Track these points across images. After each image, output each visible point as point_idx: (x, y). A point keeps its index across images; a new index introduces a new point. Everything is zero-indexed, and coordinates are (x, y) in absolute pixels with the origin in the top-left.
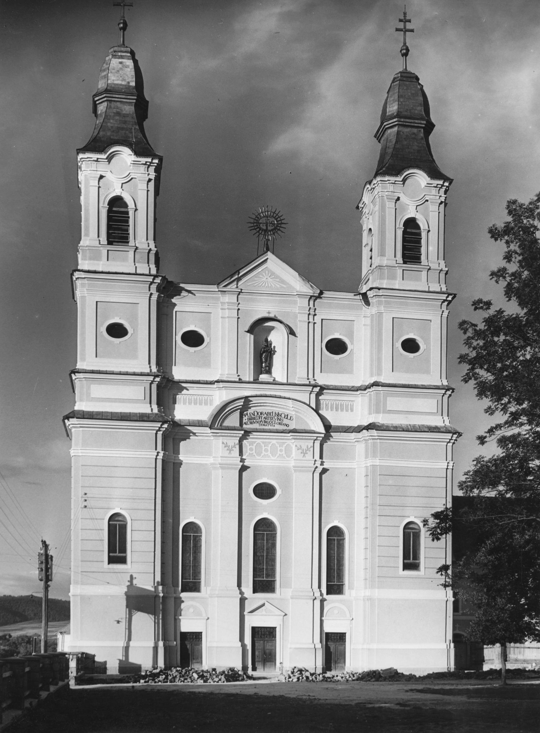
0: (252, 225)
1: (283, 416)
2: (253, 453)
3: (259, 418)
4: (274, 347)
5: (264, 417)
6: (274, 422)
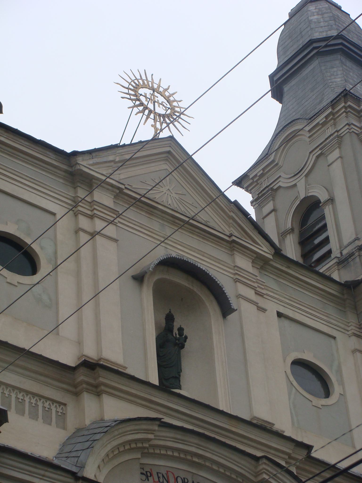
0: (126, 91)
4: (181, 330)
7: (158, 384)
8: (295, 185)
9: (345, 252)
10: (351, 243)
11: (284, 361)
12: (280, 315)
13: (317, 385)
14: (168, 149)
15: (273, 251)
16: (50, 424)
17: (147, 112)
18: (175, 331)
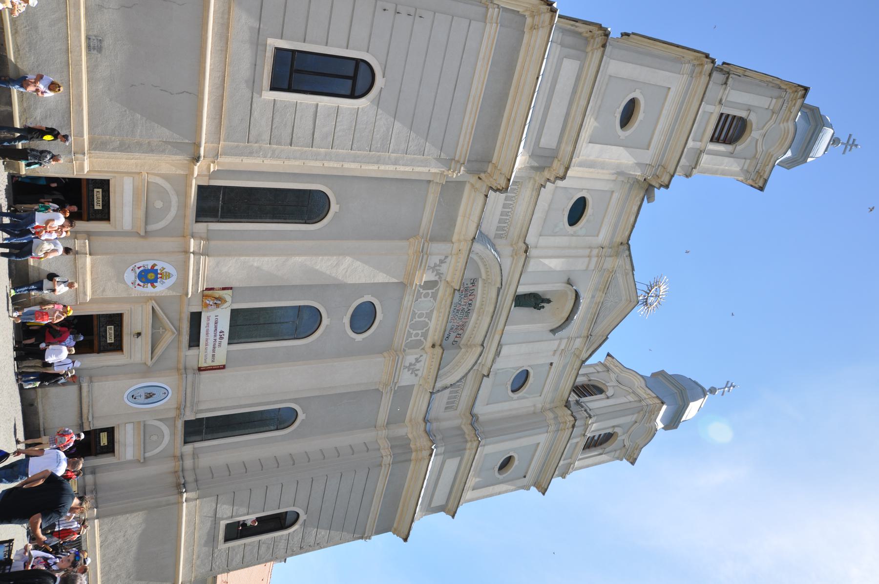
1: (460, 332)
2: (415, 318)
3: (465, 302)
4: (543, 307)
5: (464, 309)
6: (455, 321)
7: (458, 458)
8: (612, 381)
9: (582, 404)
10: (587, 406)
11: (529, 366)
12: (551, 364)
13: (517, 387)
14: (632, 301)
15: (584, 360)
16: (497, 230)
17: (648, 291)
18: (542, 304)
